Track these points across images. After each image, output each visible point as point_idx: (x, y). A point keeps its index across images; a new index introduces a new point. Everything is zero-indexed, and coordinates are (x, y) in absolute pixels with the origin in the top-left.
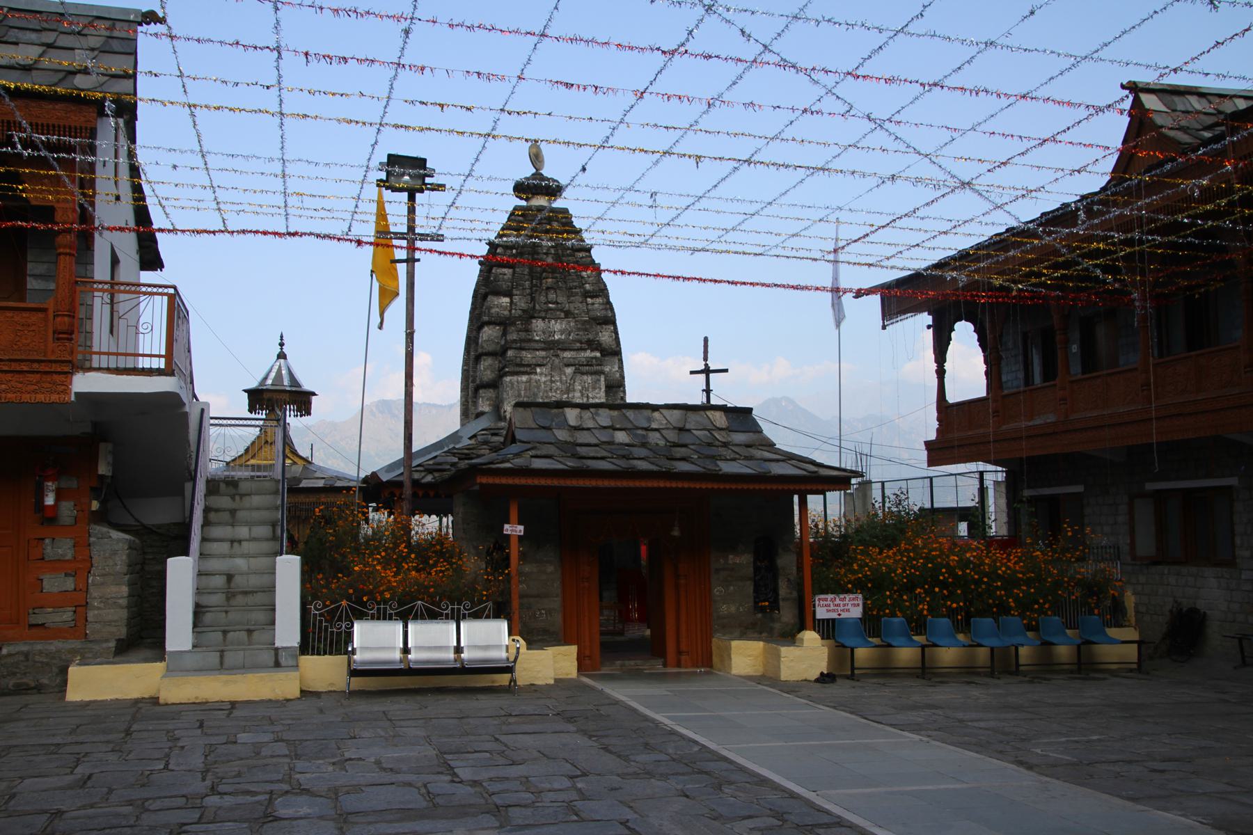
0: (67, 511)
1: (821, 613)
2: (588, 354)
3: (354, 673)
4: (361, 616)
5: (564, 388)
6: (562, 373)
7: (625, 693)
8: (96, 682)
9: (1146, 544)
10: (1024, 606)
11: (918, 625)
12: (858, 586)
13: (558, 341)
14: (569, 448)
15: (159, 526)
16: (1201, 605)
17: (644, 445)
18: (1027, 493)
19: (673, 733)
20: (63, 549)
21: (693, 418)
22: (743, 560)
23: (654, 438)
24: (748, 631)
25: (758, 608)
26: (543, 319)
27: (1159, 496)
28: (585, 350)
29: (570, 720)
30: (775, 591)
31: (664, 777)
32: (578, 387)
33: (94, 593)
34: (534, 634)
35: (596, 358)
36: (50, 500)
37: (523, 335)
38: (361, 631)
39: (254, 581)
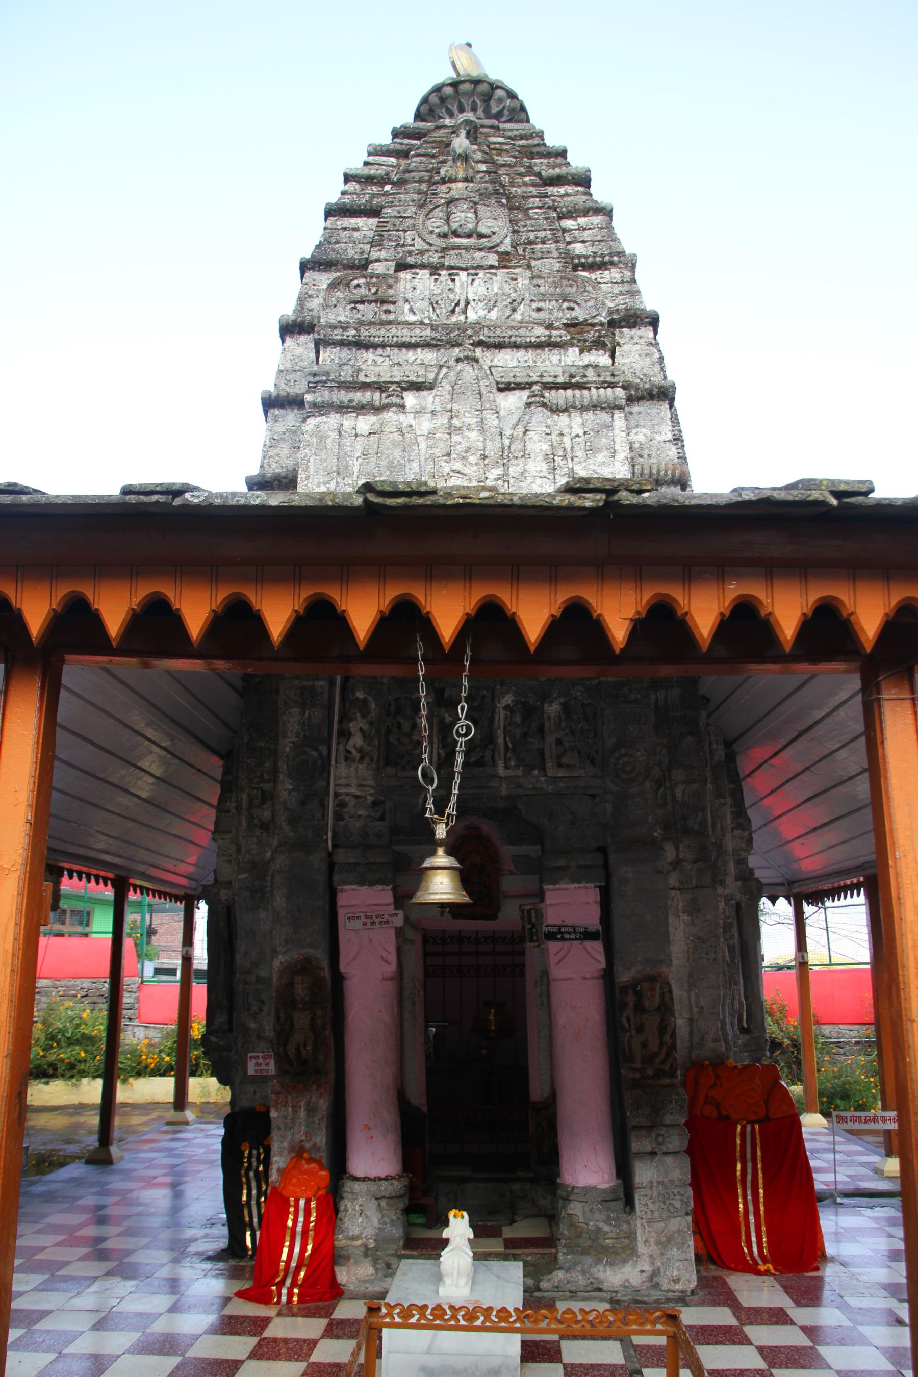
0: (357, 740)
2: (572, 357)
5: (492, 448)
13: (478, 326)
26: (435, 270)
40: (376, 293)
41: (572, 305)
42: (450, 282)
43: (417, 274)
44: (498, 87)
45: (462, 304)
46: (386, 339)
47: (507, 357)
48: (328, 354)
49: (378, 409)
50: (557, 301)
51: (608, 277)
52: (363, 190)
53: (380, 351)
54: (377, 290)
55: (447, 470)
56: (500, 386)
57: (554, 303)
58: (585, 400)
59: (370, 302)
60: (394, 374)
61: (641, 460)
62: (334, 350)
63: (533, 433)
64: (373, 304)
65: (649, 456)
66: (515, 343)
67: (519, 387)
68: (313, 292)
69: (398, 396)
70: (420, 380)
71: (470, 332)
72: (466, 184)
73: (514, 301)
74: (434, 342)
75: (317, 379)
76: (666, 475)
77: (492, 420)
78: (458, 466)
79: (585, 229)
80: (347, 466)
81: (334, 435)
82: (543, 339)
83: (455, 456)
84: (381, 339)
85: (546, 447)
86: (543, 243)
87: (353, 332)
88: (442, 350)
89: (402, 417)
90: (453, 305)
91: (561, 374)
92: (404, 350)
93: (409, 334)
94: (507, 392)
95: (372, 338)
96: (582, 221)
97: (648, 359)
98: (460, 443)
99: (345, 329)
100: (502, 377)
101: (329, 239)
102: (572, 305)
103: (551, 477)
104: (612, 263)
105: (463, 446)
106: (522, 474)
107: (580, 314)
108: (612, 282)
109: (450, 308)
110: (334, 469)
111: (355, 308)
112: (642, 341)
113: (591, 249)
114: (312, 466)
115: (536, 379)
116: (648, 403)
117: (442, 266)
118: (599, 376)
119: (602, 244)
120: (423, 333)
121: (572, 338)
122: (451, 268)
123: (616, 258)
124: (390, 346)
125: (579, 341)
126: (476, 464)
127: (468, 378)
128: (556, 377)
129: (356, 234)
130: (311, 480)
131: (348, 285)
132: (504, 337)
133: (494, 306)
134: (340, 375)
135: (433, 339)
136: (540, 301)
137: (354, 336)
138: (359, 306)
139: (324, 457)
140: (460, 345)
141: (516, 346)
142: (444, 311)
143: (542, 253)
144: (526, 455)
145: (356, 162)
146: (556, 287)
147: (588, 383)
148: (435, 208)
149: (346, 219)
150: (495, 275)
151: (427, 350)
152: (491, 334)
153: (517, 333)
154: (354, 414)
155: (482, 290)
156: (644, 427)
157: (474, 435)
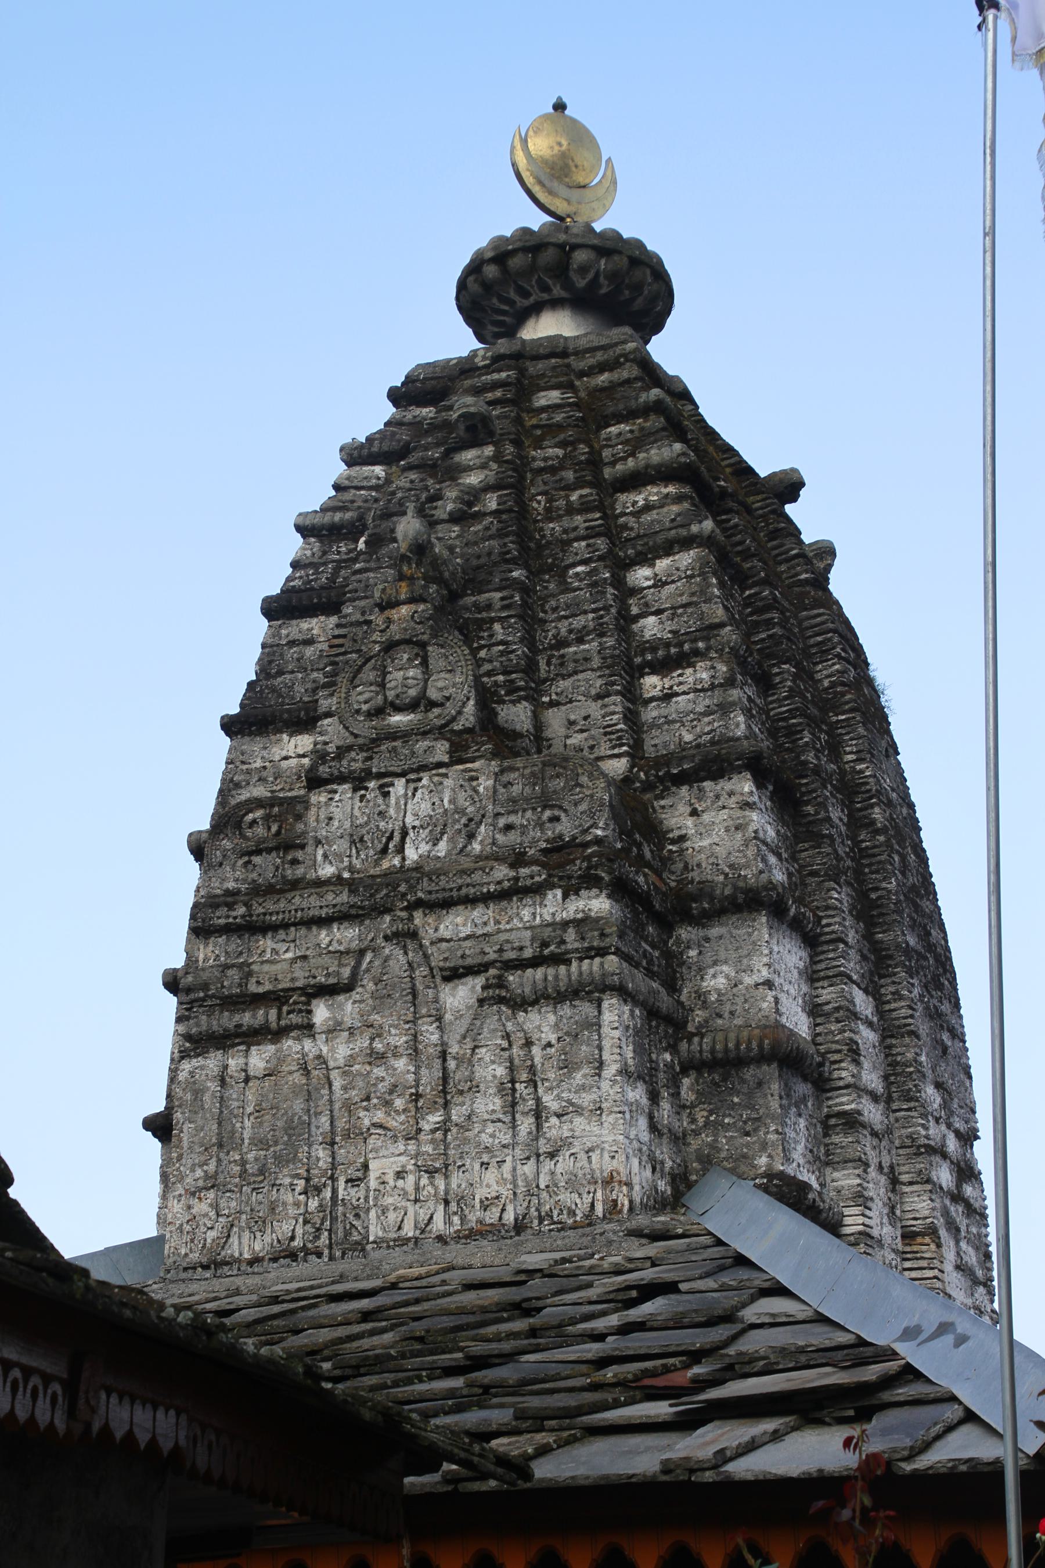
2: (554, 907)
26: (358, 781)
28: (537, 890)
32: (491, 1070)
35: (583, 923)
37: (266, 866)
40: (278, 833)
41: (556, 813)
42: (380, 801)
43: (335, 792)
44: (574, 247)
45: (397, 837)
46: (287, 915)
47: (459, 920)
48: (211, 948)
49: (278, 1034)
50: (534, 809)
51: (691, 680)
52: (324, 553)
53: (281, 934)
54: (280, 827)
55: (367, 1122)
56: (445, 973)
57: (529, 814)
58: (561, 984)
59: (269, 851)
60: (296, 975)
61: (720, 1022)
62: (220, 940)
63: (484, 1050)
64: (274, 854)
65: (732, 1013)
66: (467, 896)
67: (472, 971)
68: (242, 777)
69: (300, 1011)
70: (332, 981)
71: (403, 888)
72: (413, 607)
73: (470, 820)
74: (353, 912)
75: (192, 996)
76: (749, 1049)
77: (430, 1034)
78: (379, 1116)
79: (666, 583)
80: (233, 1132)
81: (213, 1086)
82: (506, 884)
83: (375, 1101)
84: (281, 917)
85: (501, 1071)
86: (580, 641)
87: (241, 910)
88: (367, 922)
89: (308, 1044)
90: (384, 840)
91: (528, 943)
92: (314, 928)
93: (318, 904)
94: (456, 981)
95: (268, 917)
96: (663, 564)
97: (739, 836)
98: (383, 1079)
99: (230, 906)
100: (446, 959)
101: (270, 663)
102: (556, 813)
103: (507, 1119)
104: (696, 653)
105: (386, 1083)
106: (469, 1117)
107: (566, 828)
108: (696, 691)
109: (380, 847)
110: (214, 1140)
111: (249, 862)
112: (732, 802)
113: (669, 626)
114: (185, 1139)
115: (493, 956)
116: (734, 918)
117: (368, 775)
118: (583, 939)
119: (690, 610)
120: (339, 900)
121: (550, 876)
122: (380, 776)
123: (701, 645)
124: (295, 924)
125: (561, 878)
126: (404, 1110)
127: (397, 969)
128: (521, 949)
129: (309, 652)
130: (184, 1161)
131: (238, 825)
132: (451, 890)
133: (442, 834)
134: (223, 987)
135: (352, 907)
136: (509, 813)
137: (243, 916)
138: (257, 860)
139: (200, 1123)
140: (388, 910)
141: (470, 901)
142: (371, 852)
143: (576, 661)
144: (474, 1088)
145: (315, 493)
146: (535, 784)
147: (567, 952)
148: (365, 664)
149: (294, 622)
150: (446, 775)
151: (346, 924)
152: (433, 887)
153: (469, 880)
154: (243, 1047)
155: (425, 808)
156: (726, 962)
157: (401, 1064)
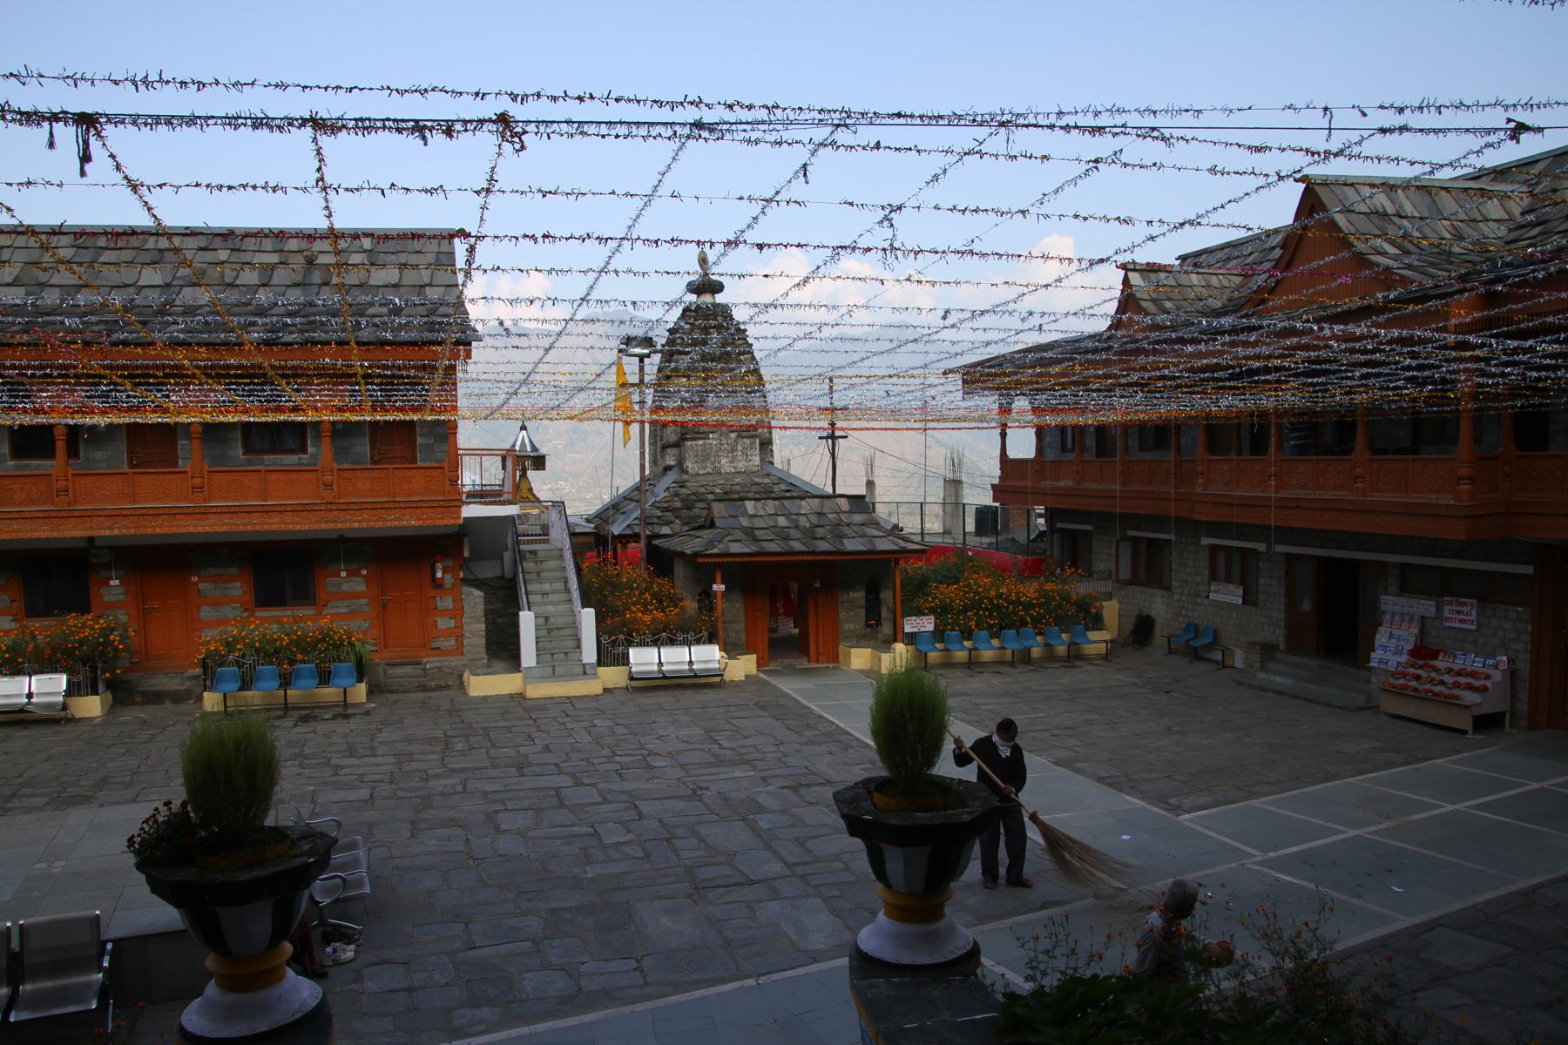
1: (908, 629)
3: (632, 679)
4: (630, 644)
6: (728, 437)
7: (789, 686)
8: (488, 685)
9: (1125, 573)
10: (1036, 621)
11: (967, 634)
12: (932, 611)
14: (750, 533)
15: (491, 579)
16: (1153, 614)
17: (797, 527)
18: (1059, 525)
19: (821, 717)
20: (446, 603)
21: (827, 502)
22: (859, 596)
23: (803, 522)
24: (861, 640)
25: (868, 625)
27: (1135, 540)
29: (763, 708)
30: (879, 613)
31: (820, 744)
33: (466, 628)
34: (731, 650)
36: (439, 575)
38: (635, 654)
39: (561, 620)
